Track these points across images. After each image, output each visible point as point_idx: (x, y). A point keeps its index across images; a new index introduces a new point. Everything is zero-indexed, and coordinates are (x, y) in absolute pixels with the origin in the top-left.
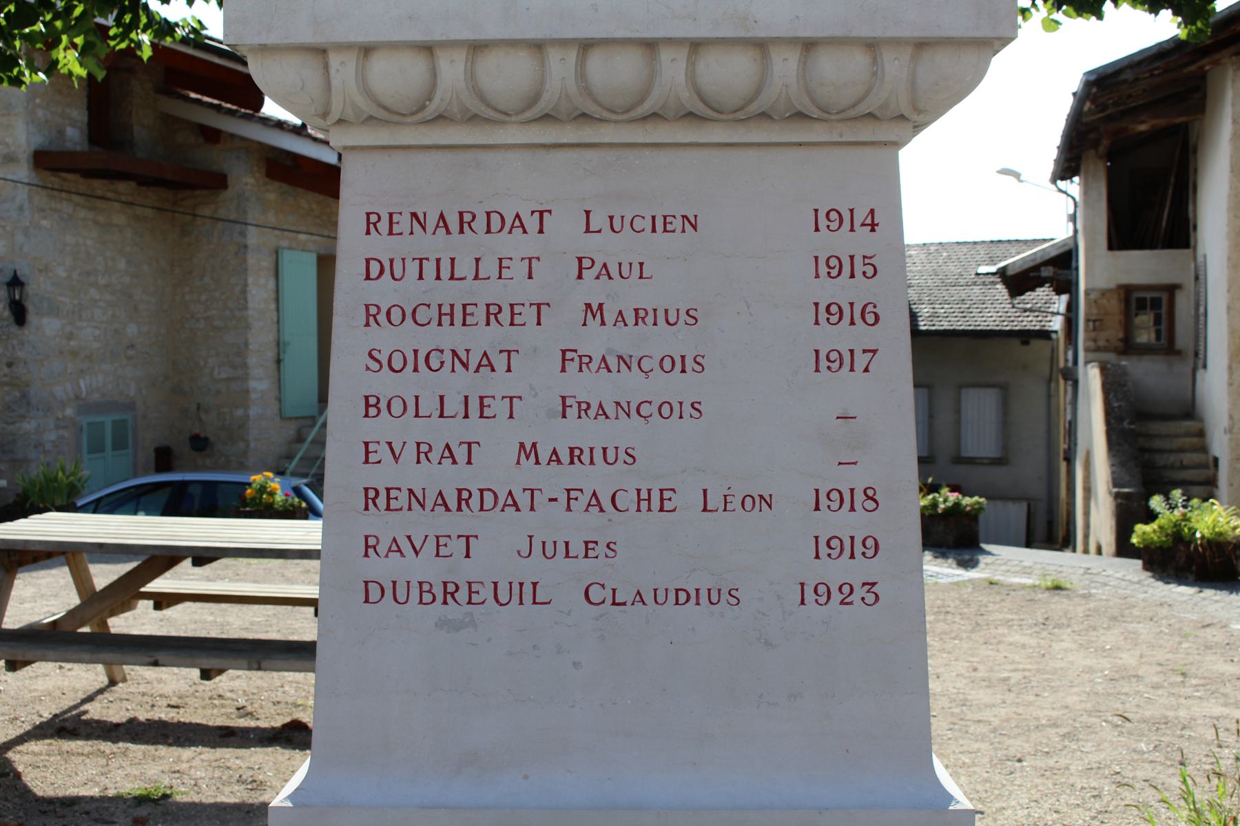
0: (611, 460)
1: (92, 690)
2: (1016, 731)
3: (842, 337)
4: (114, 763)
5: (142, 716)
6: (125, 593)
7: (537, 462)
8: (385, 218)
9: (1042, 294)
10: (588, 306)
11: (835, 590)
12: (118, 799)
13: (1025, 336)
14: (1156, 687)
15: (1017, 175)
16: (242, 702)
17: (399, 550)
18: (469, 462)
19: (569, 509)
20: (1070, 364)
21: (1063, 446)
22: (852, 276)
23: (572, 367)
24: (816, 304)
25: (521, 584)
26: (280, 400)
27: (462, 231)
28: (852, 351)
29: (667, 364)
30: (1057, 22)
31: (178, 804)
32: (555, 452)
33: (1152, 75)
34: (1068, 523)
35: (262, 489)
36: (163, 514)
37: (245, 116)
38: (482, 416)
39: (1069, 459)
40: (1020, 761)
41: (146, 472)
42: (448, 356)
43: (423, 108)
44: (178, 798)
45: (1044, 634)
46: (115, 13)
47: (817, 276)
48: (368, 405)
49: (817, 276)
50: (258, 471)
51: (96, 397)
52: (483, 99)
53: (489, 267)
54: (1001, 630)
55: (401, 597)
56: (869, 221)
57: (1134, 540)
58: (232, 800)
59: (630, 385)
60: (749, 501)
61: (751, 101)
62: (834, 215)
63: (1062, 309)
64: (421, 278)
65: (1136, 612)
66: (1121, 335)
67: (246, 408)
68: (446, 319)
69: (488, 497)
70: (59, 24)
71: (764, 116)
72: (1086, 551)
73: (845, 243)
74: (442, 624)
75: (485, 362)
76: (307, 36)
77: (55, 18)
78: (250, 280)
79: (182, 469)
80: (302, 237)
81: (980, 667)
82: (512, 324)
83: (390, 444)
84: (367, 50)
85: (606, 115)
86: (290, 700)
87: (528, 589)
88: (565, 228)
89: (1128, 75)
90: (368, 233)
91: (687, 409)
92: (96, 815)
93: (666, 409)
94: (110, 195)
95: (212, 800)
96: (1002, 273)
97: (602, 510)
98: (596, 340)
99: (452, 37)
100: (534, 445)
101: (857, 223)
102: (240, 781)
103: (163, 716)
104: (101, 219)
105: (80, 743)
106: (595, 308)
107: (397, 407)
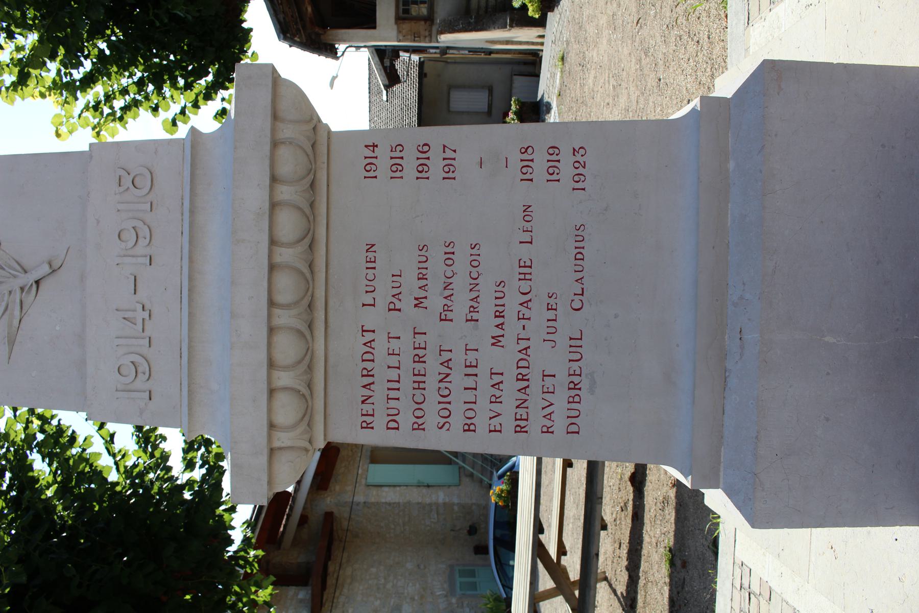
0: (502, 295)
1: (609, 590)
2: (643, 82)
3: (436, 165)
4: (651, 578)
5: (625, 563)
6: (557, 571)
7: (503, 336)
8: (365, 418)
9: (399, 65)
10: (416, 306)
11: (577, 171)
12: (671, 576)
13: (422, 75)
14: (619, 5)
15: (334, 78)
16: (618, 509)
17: (550, 414)
18: (502, 374)
19: (529, 319)
20: (438, 51)
21: (483, 55)
22: (402, 158)
23: (450, 315)
24: (418, 178)
25: (571, 346)
26: (449, 486)
27: (373, 376)
28: (444, 159)
29: (450, 262)
30: (253, 53)
31: (675, 544)
32: (497, 326)
33: (281, 4)
34: (529, 54)
35: (499, 496)
36: (514, 551)
37: (294, 501)
38: (476, 367)
39: (490, 52)
40: (660, 80)
41: (489, 559)
42: (442, 385)
43: (303, 395)
44: (671, 543)
45: (588, 66)
46: (237, 568)
47: (402, 177)
48: (469, 430)
49: (402, 177)
50: (489, 498)
51: (446, 586)
52: (299, 362)
53: (393, 361)
54: (586, 90)
55: (576, 413)
56: (371, 148)
57: (537, 16)
58: (673, 514)
59: (461, 283)
60: (527, 218)
61: (304, 212)
62: (368, 168)
63: (408, 55)
64: (398, 399)
65: (577, 17)
66: (423, 23)
67: (453, 504)
68: (422, 385)
69: (521, 364)
70: (245, 600)
71: (312, 205)
72: (542, 44)
73: (384, 162)
74: (592, 391)
75: (446, 364)
76: (264, 459)
77: (242, 602)
78: (383, 500)
79: (487, 540)
80: (360, 472)
81: (607, 101)
82: (425, 349)
83: (491, 418)
84: (272, 426)
85: (310, 293)
86: (618, 482)
87: (573, 343)
88: (371, 318)
89: (281, 16)
90: (372, 428)
91: (475, 251)
92: (680, 589)
93: (474, 263)
94: (335, 576)
95: (673, 526)
96: (387, 87)
97: (530, 300)
98: (435, 302)
99: (265, 378)
100: (493, 338)
101: (372, 155)
102: (663, 510)
103: (625, 552)
104: (349, 581)
105: (639, 597)
106: (417, 302)
107: (470, 414)
